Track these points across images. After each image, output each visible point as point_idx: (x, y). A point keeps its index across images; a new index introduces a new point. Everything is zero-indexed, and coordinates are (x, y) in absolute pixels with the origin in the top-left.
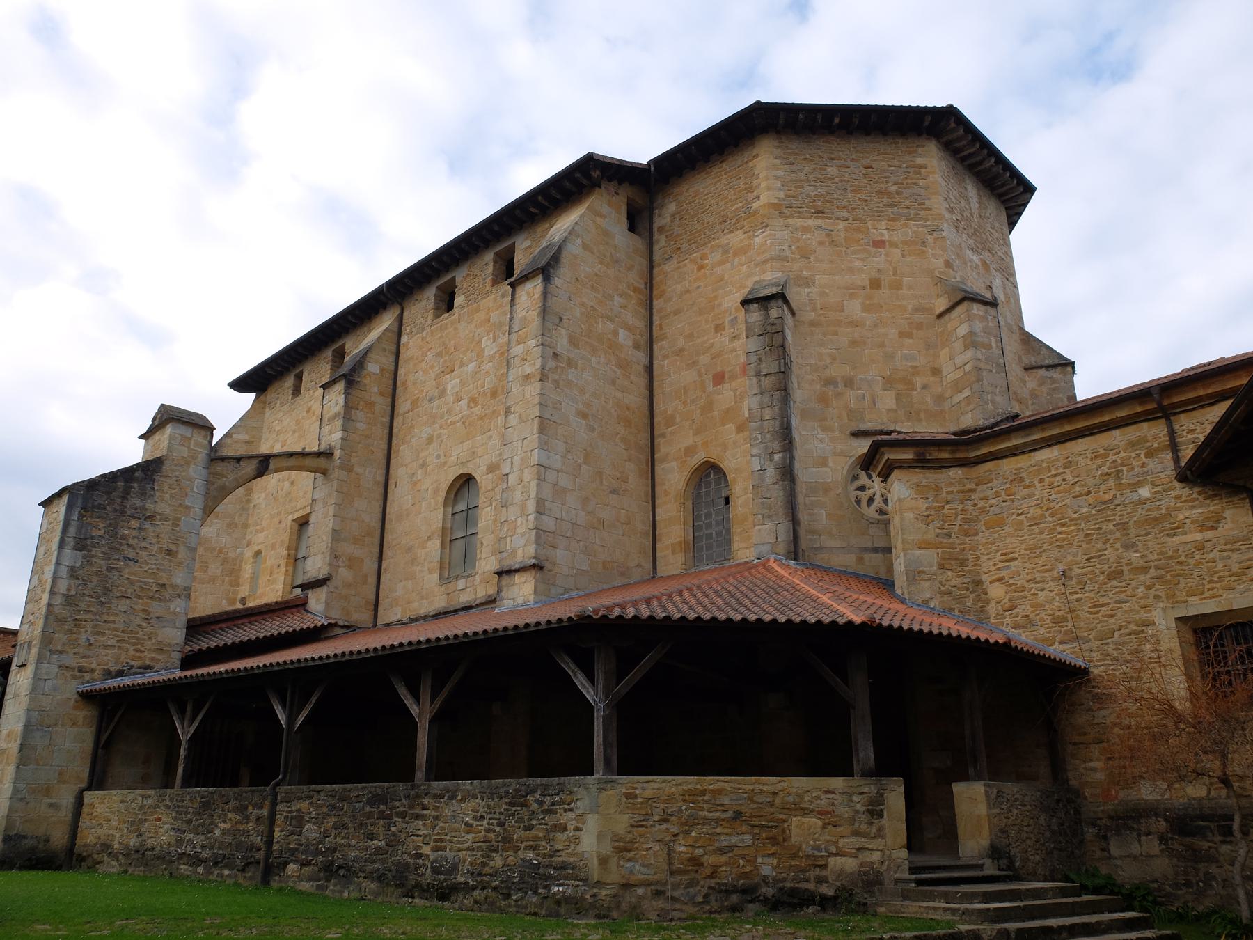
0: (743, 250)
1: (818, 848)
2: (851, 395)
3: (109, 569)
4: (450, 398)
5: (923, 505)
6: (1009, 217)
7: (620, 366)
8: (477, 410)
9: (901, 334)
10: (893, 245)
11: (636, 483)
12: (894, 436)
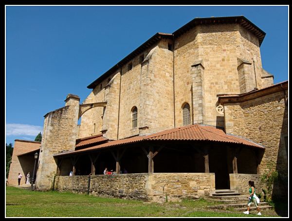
0: (193, 53)
1: (195, 188)
2: (217, 86)
3: (59, 130)
4: (131, 89)
5: (230, 111)
6: (259, 41)
7: (166, 81)
8: (137, 92)
9: (229, 72)
10: (228, 50)
11: (171, 107)
12: (225, 96)
